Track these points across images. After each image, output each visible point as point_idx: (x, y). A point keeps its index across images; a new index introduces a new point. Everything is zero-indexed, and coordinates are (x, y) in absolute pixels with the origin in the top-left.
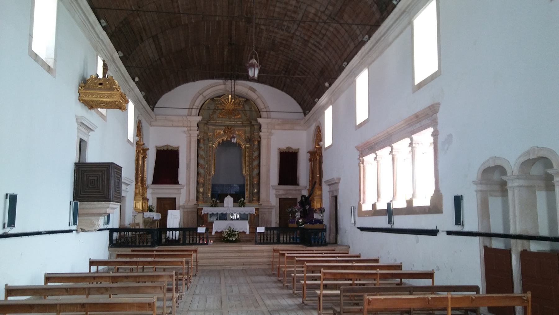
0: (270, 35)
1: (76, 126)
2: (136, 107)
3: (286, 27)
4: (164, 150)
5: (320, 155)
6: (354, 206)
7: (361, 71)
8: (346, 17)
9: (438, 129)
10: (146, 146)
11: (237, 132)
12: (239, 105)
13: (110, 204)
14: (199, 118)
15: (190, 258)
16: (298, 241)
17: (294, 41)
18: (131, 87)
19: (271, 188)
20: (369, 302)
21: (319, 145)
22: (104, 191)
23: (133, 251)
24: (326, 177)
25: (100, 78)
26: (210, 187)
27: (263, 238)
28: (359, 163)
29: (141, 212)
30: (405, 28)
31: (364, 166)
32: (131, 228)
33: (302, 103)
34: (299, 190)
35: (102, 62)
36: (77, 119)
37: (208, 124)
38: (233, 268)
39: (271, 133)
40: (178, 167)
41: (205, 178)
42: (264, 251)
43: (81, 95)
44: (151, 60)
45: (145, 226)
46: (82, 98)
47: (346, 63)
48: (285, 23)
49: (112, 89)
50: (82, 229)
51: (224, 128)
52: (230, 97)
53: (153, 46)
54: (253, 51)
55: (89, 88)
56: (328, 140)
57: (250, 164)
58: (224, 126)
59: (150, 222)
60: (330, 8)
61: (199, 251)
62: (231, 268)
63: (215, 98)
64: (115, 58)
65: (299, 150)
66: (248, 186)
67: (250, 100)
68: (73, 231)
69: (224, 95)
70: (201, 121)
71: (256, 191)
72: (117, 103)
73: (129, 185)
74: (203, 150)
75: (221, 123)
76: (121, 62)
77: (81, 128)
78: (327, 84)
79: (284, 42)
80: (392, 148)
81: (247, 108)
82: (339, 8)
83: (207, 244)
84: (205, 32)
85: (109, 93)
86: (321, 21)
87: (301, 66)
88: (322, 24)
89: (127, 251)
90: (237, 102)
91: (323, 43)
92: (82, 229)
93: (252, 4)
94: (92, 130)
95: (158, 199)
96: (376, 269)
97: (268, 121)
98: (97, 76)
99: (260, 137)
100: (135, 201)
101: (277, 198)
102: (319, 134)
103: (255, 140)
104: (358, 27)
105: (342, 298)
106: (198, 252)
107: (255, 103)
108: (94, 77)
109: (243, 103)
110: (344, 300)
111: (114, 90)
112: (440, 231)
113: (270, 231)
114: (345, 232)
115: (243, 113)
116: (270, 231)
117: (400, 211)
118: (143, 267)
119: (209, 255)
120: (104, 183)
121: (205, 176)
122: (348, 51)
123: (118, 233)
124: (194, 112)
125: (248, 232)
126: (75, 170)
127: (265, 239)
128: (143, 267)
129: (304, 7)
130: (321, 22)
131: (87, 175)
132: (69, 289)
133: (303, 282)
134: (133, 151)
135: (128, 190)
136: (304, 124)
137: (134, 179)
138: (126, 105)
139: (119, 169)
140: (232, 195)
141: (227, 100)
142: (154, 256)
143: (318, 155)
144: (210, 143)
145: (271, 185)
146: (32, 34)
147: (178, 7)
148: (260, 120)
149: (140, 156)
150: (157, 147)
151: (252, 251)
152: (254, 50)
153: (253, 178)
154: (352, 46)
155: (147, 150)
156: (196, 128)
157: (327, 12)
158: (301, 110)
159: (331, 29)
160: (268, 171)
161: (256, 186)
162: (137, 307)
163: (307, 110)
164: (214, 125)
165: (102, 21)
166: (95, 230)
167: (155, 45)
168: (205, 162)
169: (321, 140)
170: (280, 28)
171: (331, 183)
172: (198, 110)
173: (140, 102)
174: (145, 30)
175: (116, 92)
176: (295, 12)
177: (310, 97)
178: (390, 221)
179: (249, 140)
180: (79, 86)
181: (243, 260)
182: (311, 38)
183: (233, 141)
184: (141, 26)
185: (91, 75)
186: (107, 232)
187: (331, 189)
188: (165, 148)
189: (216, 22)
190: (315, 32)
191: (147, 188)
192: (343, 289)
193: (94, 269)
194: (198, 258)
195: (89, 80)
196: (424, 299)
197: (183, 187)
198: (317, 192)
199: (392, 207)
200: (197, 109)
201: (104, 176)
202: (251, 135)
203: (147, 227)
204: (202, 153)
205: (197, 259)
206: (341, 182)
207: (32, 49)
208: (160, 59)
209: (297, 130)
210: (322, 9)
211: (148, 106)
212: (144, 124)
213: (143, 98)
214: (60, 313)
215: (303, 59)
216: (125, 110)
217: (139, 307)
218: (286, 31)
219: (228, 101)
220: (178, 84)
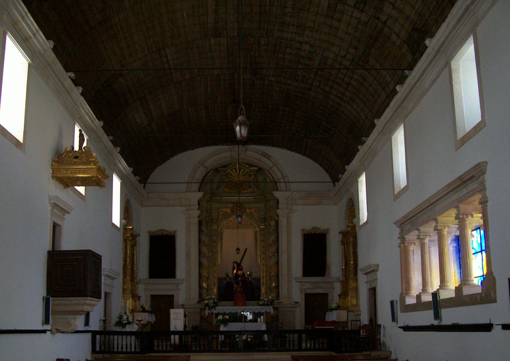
1: (49, 207)
2: (122, 184)
3: (300, 77)
5: (353, 236)
9: (487, 195)
11: (248, 211)
12: (250, 175)
13: (87, 299)
14: (200, 195)
16: (325, 346)
19: (293, 280)
21: (352, 223)
24: (362, 263)
25: (76, 151)
26: (216, 281)
30: (442, 70)
35: (79, 132)
36: (50, 200)
43: (54, 172)
50: (57, 329)
56: (364, 215)
60: (352, 51)
63: (219, 169)
66: (264, 279)
67: (264, 169)
68: (47, 332)
70: (203, 197)
72: (94, 179)
77: (55, 211)
80: (418, 230)
88: (344, 72)
90: (247, 172)
92: (57, 329)
98: (72, 149)
99: (277, 215)
100: (123, 298)
101: (301, 293)
103: (271, 219)
104: (388, 73)
109: (254, 173)
111: (91, 163)
112: (494, 325)
117: (450, 303)
124: (196, 186)
130: (343, 69)
137: (121, 271)
138: (105, 181)
139: (96, 259)
141: (234, 171)
144: (215, 225)
147: (168, 61)
148: (277, 194)
149: (129, 243)
150: (149, 232)
155: (138, 235)
156: (197, 207)
169: (355, 217)
175: (93, 166)
178: (437, 316)
185: (66, 148)
186: (89, 335)
188: (160, 233)
191: (138, 283)
195: (63, 153)
198: (352, 284)
200: (198, 183)
204: (204, 238)
210: (342, 53)
216: (104, 187)
219: (236, 171)
220: (174, 153)
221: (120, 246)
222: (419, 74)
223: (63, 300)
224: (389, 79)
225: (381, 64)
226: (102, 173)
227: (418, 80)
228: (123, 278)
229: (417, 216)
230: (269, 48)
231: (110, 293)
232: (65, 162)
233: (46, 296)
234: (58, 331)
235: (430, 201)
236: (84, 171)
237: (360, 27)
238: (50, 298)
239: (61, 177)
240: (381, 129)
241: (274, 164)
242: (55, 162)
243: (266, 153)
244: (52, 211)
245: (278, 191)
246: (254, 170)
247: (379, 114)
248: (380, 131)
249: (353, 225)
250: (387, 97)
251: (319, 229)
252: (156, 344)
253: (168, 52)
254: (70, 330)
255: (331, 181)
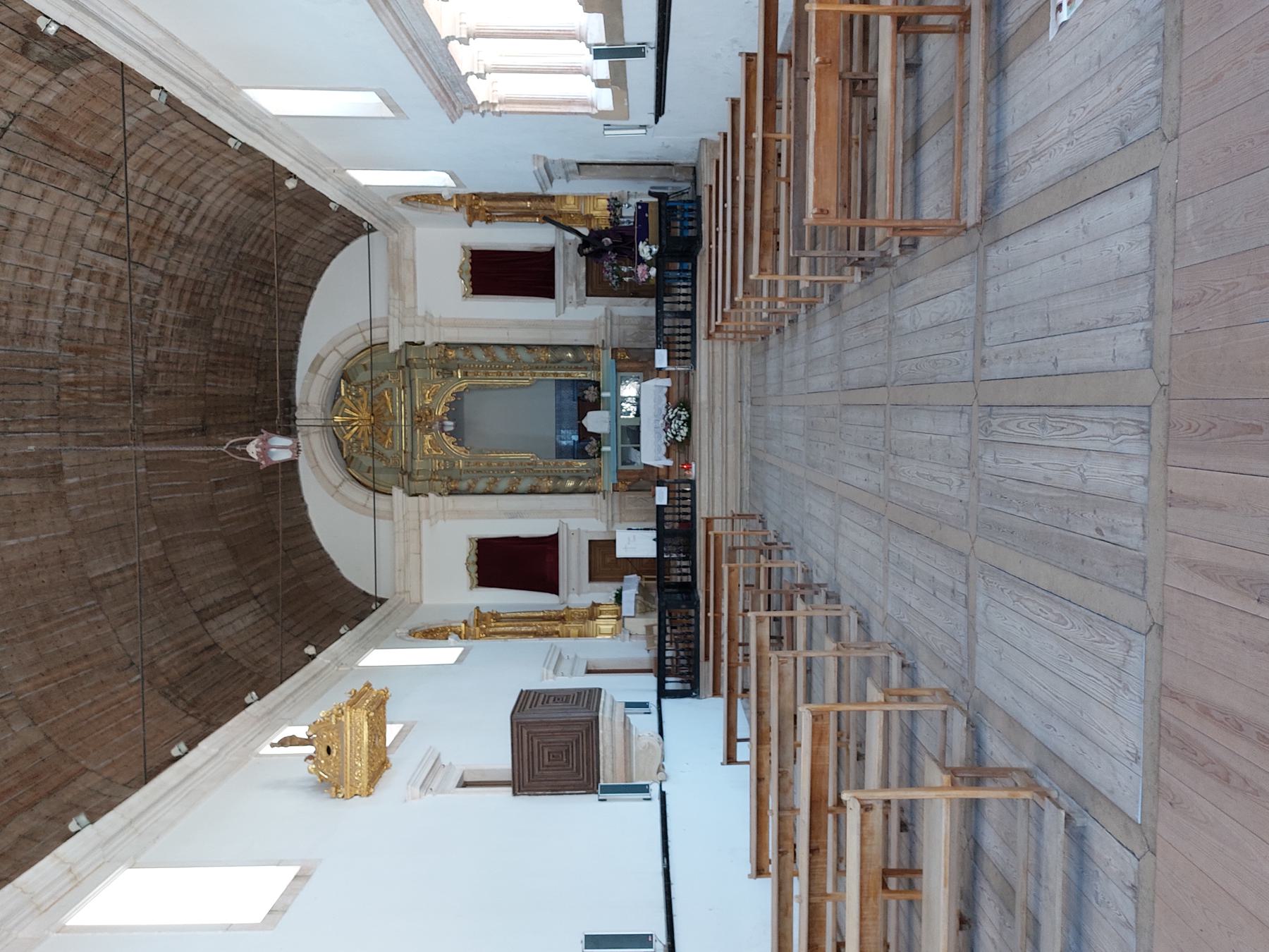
0: (172, 335)
3: (146, 297)
4: (477, 572)
5: (476, 199)
6: (602, 127)
7: (251, 105)
8: (105, 147)
10: (468, 615)
14: (398, 493)
15: (724, 537)
16: (689, 266)
17: (182, 272)
18: (329, 661)
19: (562, 317)
20: (822, 212)
21: (450, 200)
22: (576, 731)
23: (707, 658)
26: (563, 462)
27: (681, 345)
28: (494, 113)
29: (621, 621)
31: (500, 103)
32: (656, 647)
33: (343, 239)
34: (565, 247)
37: (409, 470)
38: (747, 425)
39: (425, 318)
40: (516, 539)
41: (541, 474)
42: (711, 351)
43: (357, 792)
44: (261, 619)
45: (652, 610)
46: (364, 789)
47: (231, 142)
48: (137, 300)
49: (340, 726)
51: (418, 431)
52: (338, 419)
53: (226, 618)
54: (227, 449)
55: (341, 777)
56: (436, 180)
57: (505, 368)
58: (413, 431)
59: (645, 599)
60: (83, 188)
61: (708, 513)
62: (749, 429)
63: (345, 456)
64: (264, 710)
65: (466, 245)
68: (663, 790)
69: (336, 433)
70: (403, 488)
71: (570, 355)
73: (560, 653)
74: (475, 482)
75: (406, 439)
76: (272, 695)
78: (291, 184)
79: (187, 296)
81: (364, 376)
82: (81, 166)
83: (692, 483)
84: (180, 495)
85: (348, 733)
86: (122, 209)
87: (246, 248)
89: (706, 669)
90: (352, 401)
91: (182, 197)
93: (93, 388)
94: (438, 759)
95: (586, 936)
96: (754, 141)
97: (394, 323)
102: (425, 199)
103: (445, 356)
104: (130, 115)
105: (819, 253)
106: (711, 516)
107: (349, 357)
108: (314, 766)
110: (823, 249)
113: (666, 303)
114: (668, 147)
115: (377, 385)
116: (666, 303)
117: (614, 25)
118: (740, 644)
119: (718, 478)
120: (557, 732)
121: (538, 474)
122: (197, 135)
123: (667, 679)
125: (667, 382)
126: (529, 795)
127: (682, 347)
128: (740, 644)
129: (88, 256)
131: (539, 770)
132: (781, 850)
133: (781, 304)
134: (483, 647)
135: (572, 656)
136: (397, 232)
139: (526, 700)
140: (582, 415)
142: (716, 615)
143: (477, 205)
145: (556, 319)
146: (224, 924)
147: (120, 571)
150: (471, 588)
151: (711, 381)
152: (225, 447)
153: (538, 360)
154: (181, 126)
155: (478, 611)
156: (421, 498)
157: (96, 196)
158: (364, 238)
159: (141, 181)
160: (521, 324)
161: (558, 355)
162: (819, 744)
163: (362, 226)
164: (413, 458)
165: (175, 752)
166: (659, 743)
167: (222, 614)
168: (504, 477)
170: (149, 312)
171: (547, 179)
172: (377, 495)
173: (364, 636)
174: (187, 644)
175: (346, 717)
176: (105, 277)
177: (325, 221)
178: (638, 52)
179: (446, 371)
180: (337, 797)
181: (731, 403)
182: (171, 229)
183: (452, 429)
184: (177, 653)
185: (310, 772)
186: (666, 703)
187: (562, 174)
188: (474, 568)
189: (149, 473)
190: (151, 221)
192: (796, 251)
193: (744, 751)
194: (724, 516)
196: (819, 73)
197: (565, 526)
199: (603, 45)
201: (542, 732)
202: (432, 366)
203: (656, 606)
204: (482, 485)
205: (726, 518)
206: (542, 154)
207: (259, 922)
208: (256, 598)
209: (414, 249)
210: (89, 208)
211: (374, 614)
212: (421, 619)
213: (354, 630)
214: (827, 895)
215: (228, 244)
217: (820, 740)
218: (157, 294)
221: (497, 644)
222: (129, 48)
223: (604, 762)
224: (144, 113)
225: (111, 128)
226: (359, 698)
227: (146, 52)
228: (559, 637)
229: (439, 77)
230: (84, 363)
231: (587, 663)
232: (337, 773)
233: (596, 796)
234: (661, 769)
235: (409, 50)
236: (357, 734)
237: (26, 170)
238: (601, 786)
239: (369, 777)
240: (256, 135)
241: (335, 349)
242: (337, 793)
243: (313, 364)
244: (436, 791)
245: (387, 343)
246: (346, 389)
247: (221, 136)
248: (261, 138)
249: (455, 200)
250: (185, 119)
251: (463, 264)
252: (679, 579)
253: (99, 572)
254: (658, 747)
255: (366, 236)
